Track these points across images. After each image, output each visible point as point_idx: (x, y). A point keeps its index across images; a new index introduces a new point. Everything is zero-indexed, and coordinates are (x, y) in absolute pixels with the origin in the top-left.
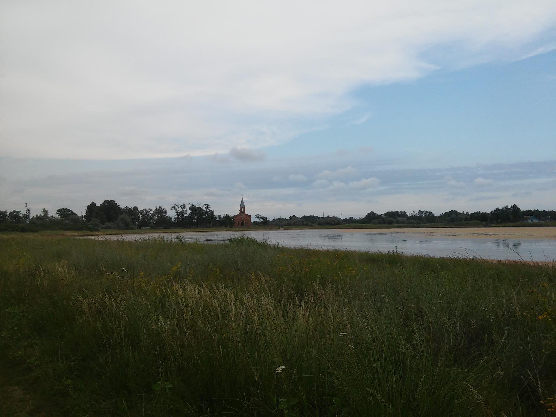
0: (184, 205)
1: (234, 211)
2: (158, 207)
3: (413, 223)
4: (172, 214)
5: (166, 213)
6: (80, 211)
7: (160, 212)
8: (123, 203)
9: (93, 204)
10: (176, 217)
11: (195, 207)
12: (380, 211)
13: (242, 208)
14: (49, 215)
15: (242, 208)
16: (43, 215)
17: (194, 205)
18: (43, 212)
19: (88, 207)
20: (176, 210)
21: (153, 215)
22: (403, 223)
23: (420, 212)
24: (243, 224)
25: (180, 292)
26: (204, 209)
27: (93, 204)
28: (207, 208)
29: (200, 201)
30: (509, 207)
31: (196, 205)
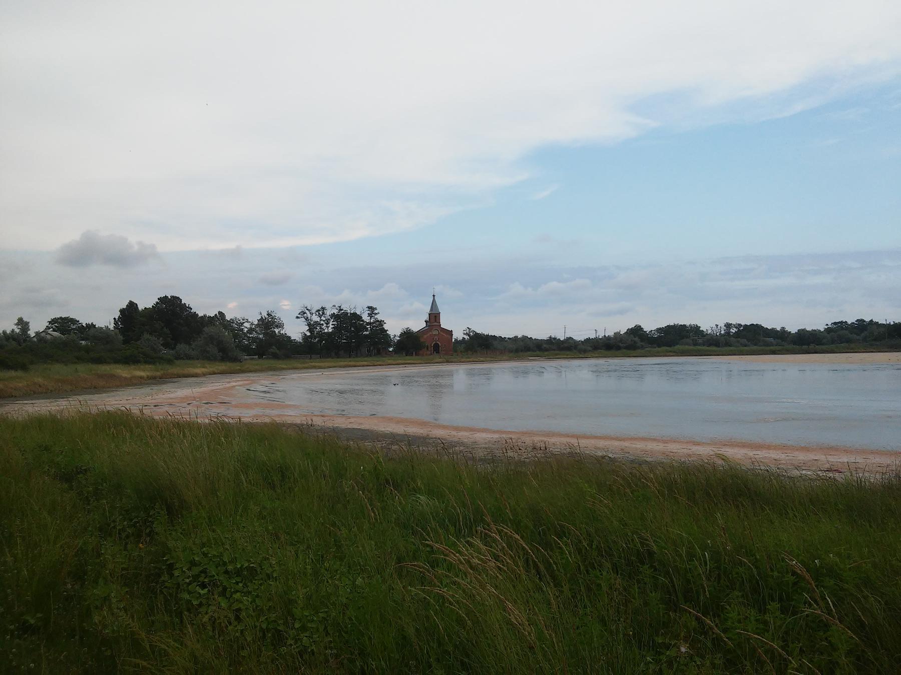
0: (323, 309)
1: (417, 324)
2: (265, 314)
3: (771, 344)
4: (295, 330)
5: (280, 326)
6: (295, 330)
7: (268, 323)
8: (202, 305)
9: (132, 305)
10: (308, 334)
11: (346, 314)
12: (651, 324)
13: (434, 317)
14: (32, 333)
15: (434, 317)
16: (17, 331)
17: (344, 307)
18: (17, 324)
19: (122, 311)
20: (307, 319)
21: (251, 330)
22: (767, 344)
23: (728, 326)
24: (436, 349)
25: (462, 448)
26: (366, 318)
27: (132, 305)
28: (370, 315)
29: (356, 304)
30: (849, 323)
31: (348, 308)
